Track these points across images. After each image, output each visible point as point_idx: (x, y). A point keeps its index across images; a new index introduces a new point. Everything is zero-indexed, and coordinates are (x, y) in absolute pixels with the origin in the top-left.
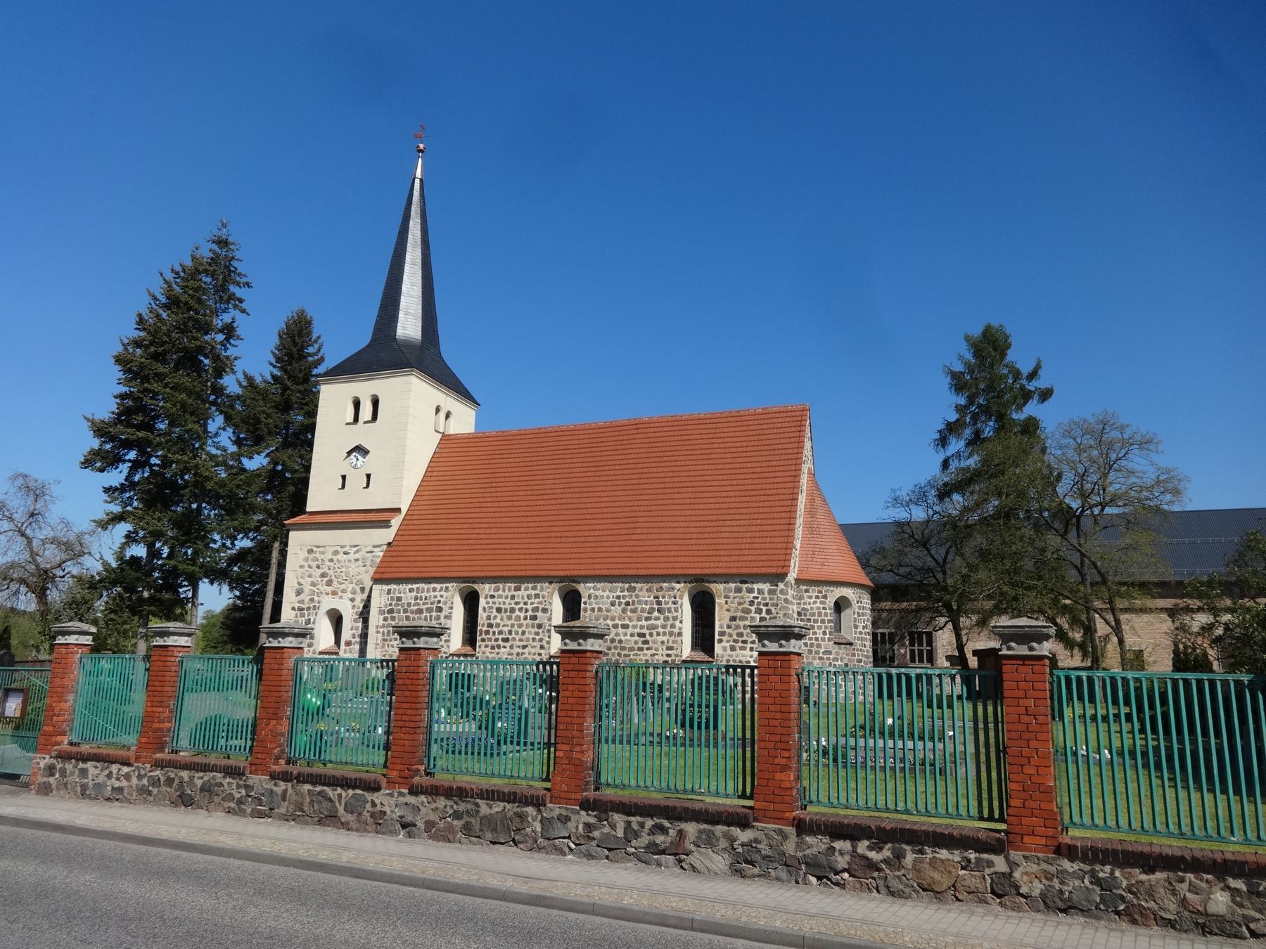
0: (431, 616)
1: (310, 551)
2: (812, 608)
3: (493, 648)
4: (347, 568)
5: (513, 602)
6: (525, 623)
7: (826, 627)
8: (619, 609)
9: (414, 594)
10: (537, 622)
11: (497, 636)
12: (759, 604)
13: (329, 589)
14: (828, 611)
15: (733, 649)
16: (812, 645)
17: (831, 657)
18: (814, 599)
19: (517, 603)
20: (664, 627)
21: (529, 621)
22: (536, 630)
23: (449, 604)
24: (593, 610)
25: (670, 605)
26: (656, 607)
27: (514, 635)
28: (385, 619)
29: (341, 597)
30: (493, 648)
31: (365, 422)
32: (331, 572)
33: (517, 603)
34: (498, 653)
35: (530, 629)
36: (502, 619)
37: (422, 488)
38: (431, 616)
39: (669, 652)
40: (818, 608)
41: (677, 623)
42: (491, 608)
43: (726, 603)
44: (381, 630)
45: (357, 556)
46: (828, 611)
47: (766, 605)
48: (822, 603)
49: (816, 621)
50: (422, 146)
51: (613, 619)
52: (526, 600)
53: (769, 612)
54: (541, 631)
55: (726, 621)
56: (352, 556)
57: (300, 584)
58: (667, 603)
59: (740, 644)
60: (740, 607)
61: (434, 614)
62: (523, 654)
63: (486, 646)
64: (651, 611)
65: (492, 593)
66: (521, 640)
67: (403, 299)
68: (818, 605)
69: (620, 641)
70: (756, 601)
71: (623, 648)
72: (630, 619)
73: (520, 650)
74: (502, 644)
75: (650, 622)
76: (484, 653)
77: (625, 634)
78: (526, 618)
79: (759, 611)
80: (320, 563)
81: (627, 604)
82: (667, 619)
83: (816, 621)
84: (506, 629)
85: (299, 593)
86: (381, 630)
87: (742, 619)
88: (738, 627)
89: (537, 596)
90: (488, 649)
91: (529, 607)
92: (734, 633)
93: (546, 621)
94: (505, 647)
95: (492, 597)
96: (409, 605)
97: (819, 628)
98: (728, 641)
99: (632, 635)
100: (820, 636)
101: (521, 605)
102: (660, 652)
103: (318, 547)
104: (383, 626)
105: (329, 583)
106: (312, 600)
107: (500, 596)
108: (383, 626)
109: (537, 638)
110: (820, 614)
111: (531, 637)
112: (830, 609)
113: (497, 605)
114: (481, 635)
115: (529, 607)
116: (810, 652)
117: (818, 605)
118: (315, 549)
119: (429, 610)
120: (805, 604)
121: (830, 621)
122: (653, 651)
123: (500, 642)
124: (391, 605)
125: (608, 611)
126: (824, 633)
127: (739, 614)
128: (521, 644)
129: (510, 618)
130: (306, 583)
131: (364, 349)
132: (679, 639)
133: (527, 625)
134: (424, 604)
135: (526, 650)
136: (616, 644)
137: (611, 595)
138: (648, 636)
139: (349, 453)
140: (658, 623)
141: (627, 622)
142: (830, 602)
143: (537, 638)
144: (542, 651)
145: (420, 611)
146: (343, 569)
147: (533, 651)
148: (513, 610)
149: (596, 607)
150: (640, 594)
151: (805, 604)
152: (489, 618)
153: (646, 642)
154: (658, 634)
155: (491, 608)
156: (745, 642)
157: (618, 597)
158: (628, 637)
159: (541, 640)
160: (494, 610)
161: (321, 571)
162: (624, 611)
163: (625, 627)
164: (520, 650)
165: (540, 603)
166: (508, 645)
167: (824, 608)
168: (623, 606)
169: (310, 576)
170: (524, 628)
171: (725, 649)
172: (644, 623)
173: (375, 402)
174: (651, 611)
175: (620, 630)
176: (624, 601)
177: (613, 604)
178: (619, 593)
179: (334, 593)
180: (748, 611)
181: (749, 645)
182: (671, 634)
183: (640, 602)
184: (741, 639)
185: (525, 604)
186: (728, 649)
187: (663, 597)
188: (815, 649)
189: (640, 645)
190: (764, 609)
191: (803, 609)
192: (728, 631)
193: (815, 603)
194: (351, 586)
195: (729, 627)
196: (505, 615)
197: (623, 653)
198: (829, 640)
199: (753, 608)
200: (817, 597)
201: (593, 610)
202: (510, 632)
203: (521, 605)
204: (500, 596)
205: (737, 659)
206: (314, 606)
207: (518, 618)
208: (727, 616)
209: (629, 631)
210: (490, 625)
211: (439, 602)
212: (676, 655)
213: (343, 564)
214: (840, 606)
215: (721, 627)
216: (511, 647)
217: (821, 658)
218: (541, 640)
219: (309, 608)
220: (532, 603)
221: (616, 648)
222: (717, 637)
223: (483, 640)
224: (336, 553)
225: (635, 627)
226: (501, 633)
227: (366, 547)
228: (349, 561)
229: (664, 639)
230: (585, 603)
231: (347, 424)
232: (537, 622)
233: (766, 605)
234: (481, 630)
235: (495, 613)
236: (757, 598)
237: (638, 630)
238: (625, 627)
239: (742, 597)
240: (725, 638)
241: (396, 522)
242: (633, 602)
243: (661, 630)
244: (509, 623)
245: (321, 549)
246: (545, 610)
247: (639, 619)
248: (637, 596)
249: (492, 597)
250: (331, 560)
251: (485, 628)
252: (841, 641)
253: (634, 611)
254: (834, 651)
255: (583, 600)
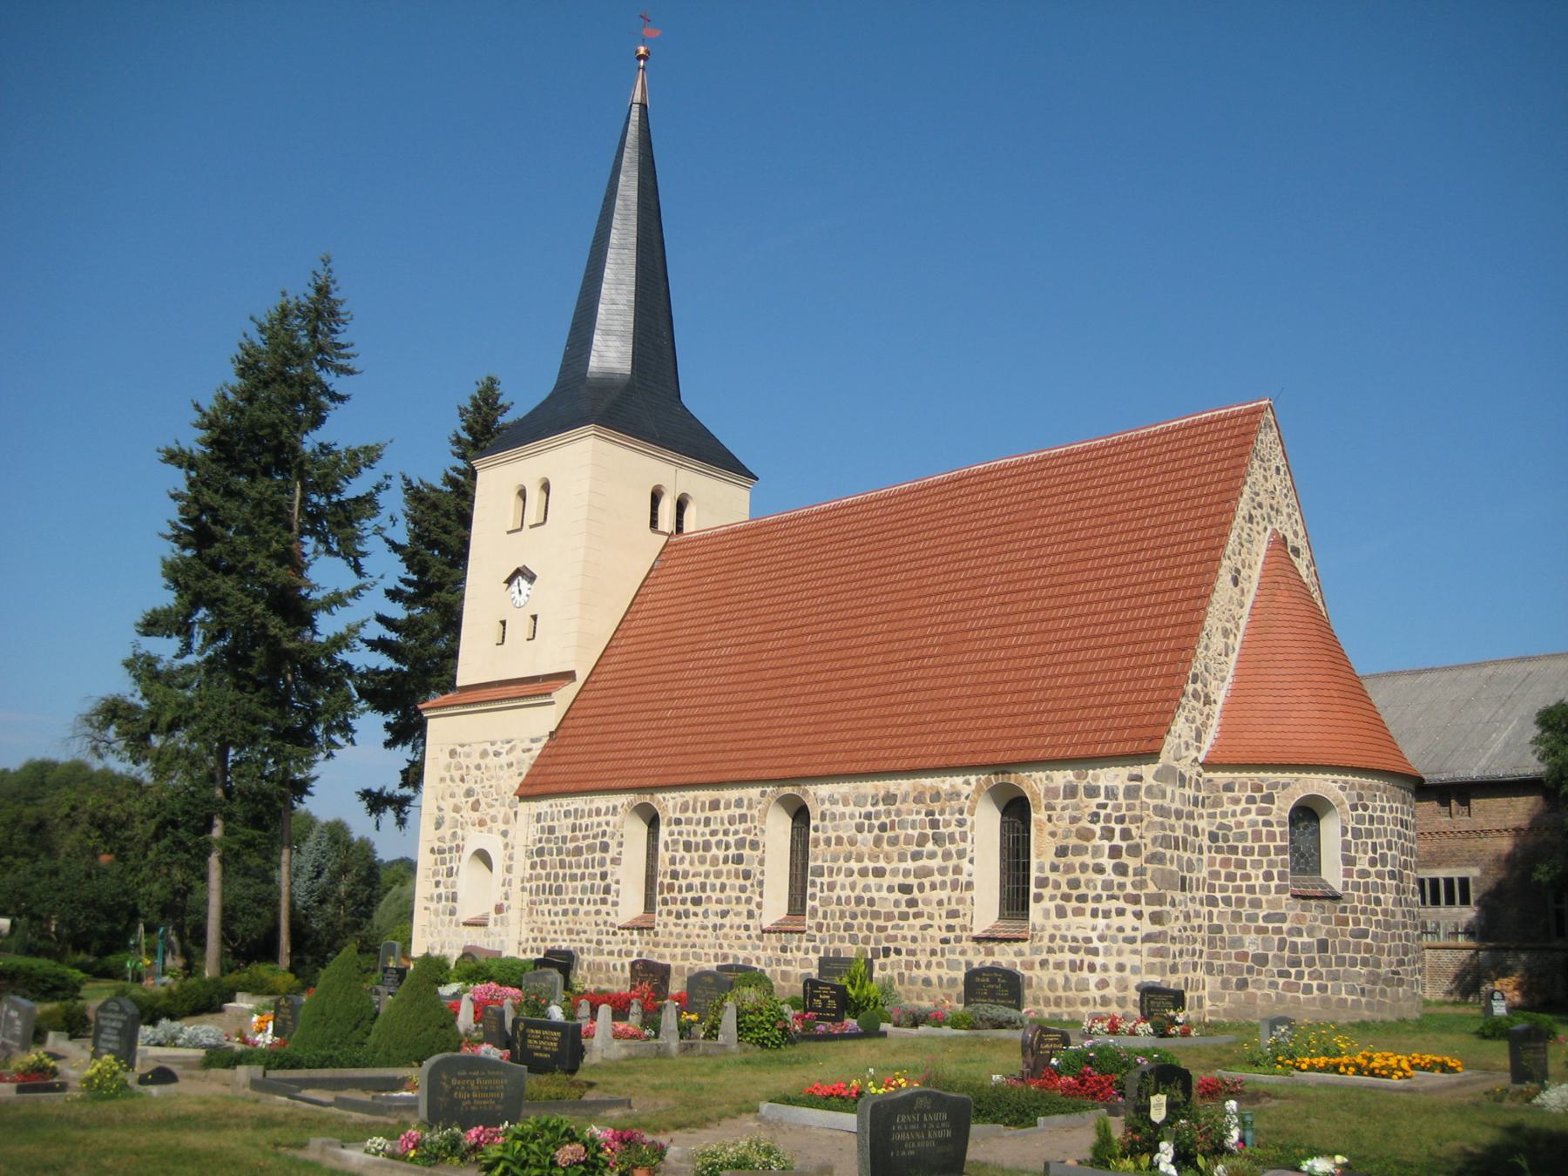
0: (593, 860)
1: (453, 753)
2: (1239, 825)
3: (678, 916)
4: (499, 779)
5: (707, 830)
6: (724, 868)
7: (1271, 864)
8: (870, 837)
9: (571, 820)
10: (742, 867)
11: (684, 894)
12: (1108, 818)
13: (476, 816)
14: (1277, 829)
15: (1061, 913)
16: (1240, 902)
17: (1285, 926)
18: (1243, 804)
19: (714, 833)
20: (943, 871)
21: (731, 866)
22: (741, 881)
23: (617, 838)
24: (828, 841)
25: (953, 828)
26: (929, 832)
27: (709, 893)
28: (533, 866)
29: (490, 831)
30: (678, 916)
31: (531, 527)
32: (477, 788)
33: (714, 833)
34: (686, 926)
35: (733, 881)
36: (692, 863)
37: (619, 634)
38: (593, 860)
39: (952, 922)
40: (1253, 823)
41: (965, 863)
42: (675, 842)
43: (1050, 819)
44: (527, 885)
45: (511, 758)
46: (1277, 829)
47: (1121, 820)
48: (1261, 812)
49: (1248, 851)
50: (642, 50)
51: (860, 859)
52: (727, 825)
53: (1126, 834)
54: (748, 883)
55: (1050, 857)
56: (504, 759)
57: (440, 809)
58: (948, 825)
59: (1074, 904)
60: (1074, 828)
61: (598, 855)
62: (722, 926)
63: (669, 913)
64: (922, 840)
65: (678, 815)
66: (719, 901)
67: (601, 308)
68: (1253, 816)
69: (871, 902)
70: (1102, 813)
71: (876, 915)
72: (888, 858)
73: (718, 921)
74: (692, 908)
75: (920, 863)
76: (666, 925)
77: (879, 889)
78: (726, 861)
79: (1108, 833)
80: (464, 772)
81: (883, 828)
82: (947, 856)
83: (1248, 851)
84: (697, 881)
85: (438, 825)
86: (527, 885)
87: (1079, 851)
88: (1069, 868)
89: (743, 818)
90: (672, 919)
91: (731, 839)
92: (1063, 880)
93: (756, 865)
94: (695, 914)
95: (678, 822)
96: (564, 839)
97: (1257, 865)
98: (1052, 898)
99: (890, 889)
100: (1258, 882)
101: (720, 836)
102: (935, 923)
103: (462, 746)
104: (530, 879)
105: (475, 807)
106: (454, 835)
107: (689, 821)
108: (530, 879)
109: (744, 896)
110: (1257, 836)
111: (734, 894)
112: (1280, 824)
113: (685, 837)
114: (661, 892)
115: (731, 839)
116: (1237, 916)
117: (1253, 816)
118: (459, 749)
119: (591, 848)
120: (1224, 815)
121: (1279, 850)
122: (924, 921)
123: (689, 906)
124: (540, 841)
125: (852, 842)
126: (1268, 876)
127: (1073, 841)
128: (719, 908)
129: (702, 861)
130: (447, 805)
131: (543, 404)
132: (967, 895)
133: (729, 872)
134: (585, 837)
135: (727, 921)
136: (864, 906)
137: (857, 810)
138: (915, 890)
139: (509, 581)
140: (935, 863)
141: (882, 863)
142: (1282, 807)
143: (744, 896)
144: (750, 922)
145: (578, 851)
146: (493, 782)
147: (737, 921)
148: (707, 846)
149: (833, 835)
150: (904, 807)
151: (1224, 815)
152: (673, 861)
153: (912, 903)
154: (933, 887)
155: (675, 842)
156: (1082, 898)
157: (868, 816)
158: (884, 893)
159: (749, 901)
160: (681, 847)
161: (465, 786)
162: (878, 842)
163: (879, 873)
164: (718, 921)
165: (747, 831)
166: (700, 910)
167: (1267, 823)
168: (876, 831)
169: (452, 795)
170: (724, 879)
171: (1046, 913)
172: (910, 864)
173: (546, 487)
174: (922, 840)
175: (871, 880)
176: (876, 823)
177: (860, 828)
178: (869, 808)
179: (482, 823)
180: (1086, 835)
181: (1089, 906)
182: (955, 885)
183: (902, 825)
184: (1075, 893)
185: (726, 833)
186: (1053, 913)
187: (942, 812)
188: (1246, 910)
189: (904, 908)
190: (1118, 828)
191: (1222, 826)
192: (1052, 876)
193: (1246, 812)
194: (503, 810)
195: (1054, 868)
196: (695, 855)
197: (875, 923)
198: (1279, 890)
199: (1097, 828)
200: (1251, 800)
201: (828, 841)
202: (703, 887)
203: (720, 836)
204: (689, 821)
205: (1069, 934)
206: (458, 846)
207: (715, 861)
208: (1051, 846)
209: (887, 881)
210: (674, 875)
211: (604, 834)
212: (963, 928)
213: (492, 772)
214: (1308, 813)
215: (1041, 868)
216: (705, 914)
217: (1260, 930)
218: (749, 901)
219: (451, 849)
220: (736, 832)
221: (864, 914)
222: (1033, 890)
223: (665, 902)
224: (484, 754)
225: (895, 872)
226: (690, 888)
227: (522, 741)
228: (501, 767)
229: (943, 894)
230: (816, 829)
231: (509, 532)
232: (742, 867)
233: (1121, 820)
234: (662, 883)
235: (681, 852)
236: (1104, 806)
237: (900, 879)
238: (879, 873)
239: (1077, 807)
240: (1047, 892)
241: (565, 695)
242: (893, 822)
243: (937, 878)
244: (702, 869)
245: (466, 749)
246: (754, 845)
247: (902, 858)
248: (898, 813)
249: (678, 822)
250: (478, 767)
251: (668, 880)
252: (1310, 891)
253: (893, 841)
254: (1291, 914)
255: (813, 823)
